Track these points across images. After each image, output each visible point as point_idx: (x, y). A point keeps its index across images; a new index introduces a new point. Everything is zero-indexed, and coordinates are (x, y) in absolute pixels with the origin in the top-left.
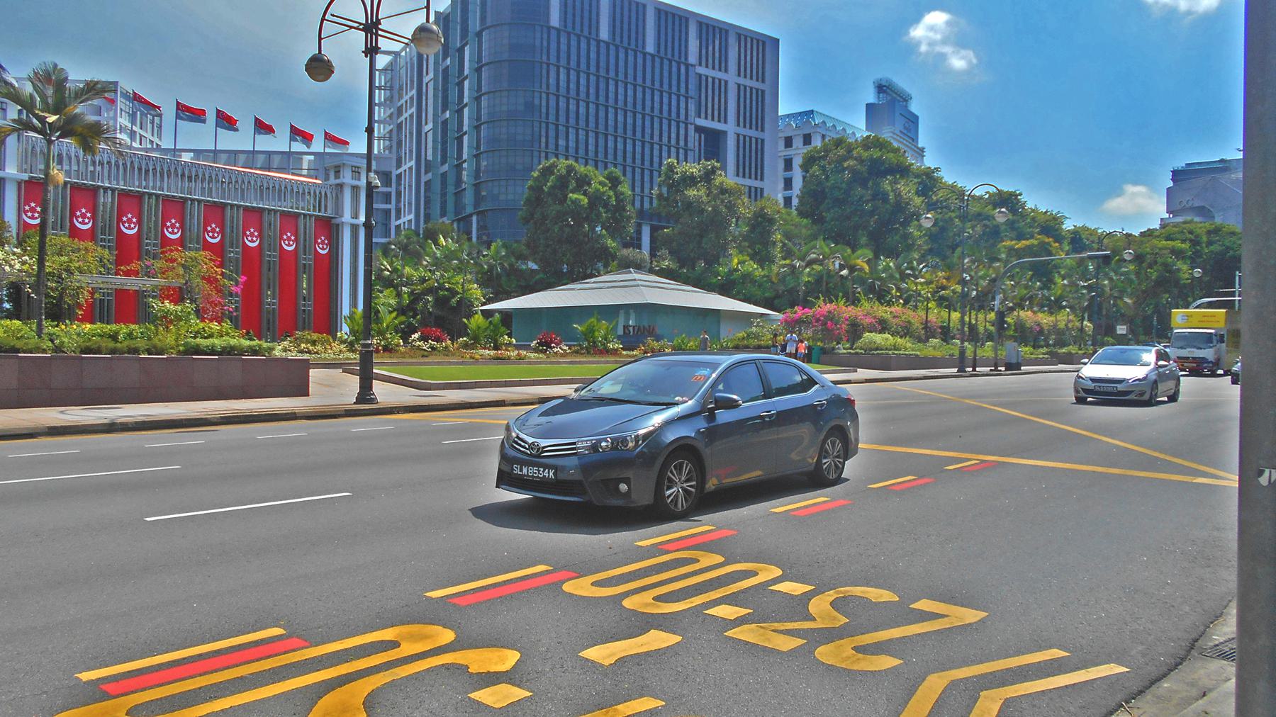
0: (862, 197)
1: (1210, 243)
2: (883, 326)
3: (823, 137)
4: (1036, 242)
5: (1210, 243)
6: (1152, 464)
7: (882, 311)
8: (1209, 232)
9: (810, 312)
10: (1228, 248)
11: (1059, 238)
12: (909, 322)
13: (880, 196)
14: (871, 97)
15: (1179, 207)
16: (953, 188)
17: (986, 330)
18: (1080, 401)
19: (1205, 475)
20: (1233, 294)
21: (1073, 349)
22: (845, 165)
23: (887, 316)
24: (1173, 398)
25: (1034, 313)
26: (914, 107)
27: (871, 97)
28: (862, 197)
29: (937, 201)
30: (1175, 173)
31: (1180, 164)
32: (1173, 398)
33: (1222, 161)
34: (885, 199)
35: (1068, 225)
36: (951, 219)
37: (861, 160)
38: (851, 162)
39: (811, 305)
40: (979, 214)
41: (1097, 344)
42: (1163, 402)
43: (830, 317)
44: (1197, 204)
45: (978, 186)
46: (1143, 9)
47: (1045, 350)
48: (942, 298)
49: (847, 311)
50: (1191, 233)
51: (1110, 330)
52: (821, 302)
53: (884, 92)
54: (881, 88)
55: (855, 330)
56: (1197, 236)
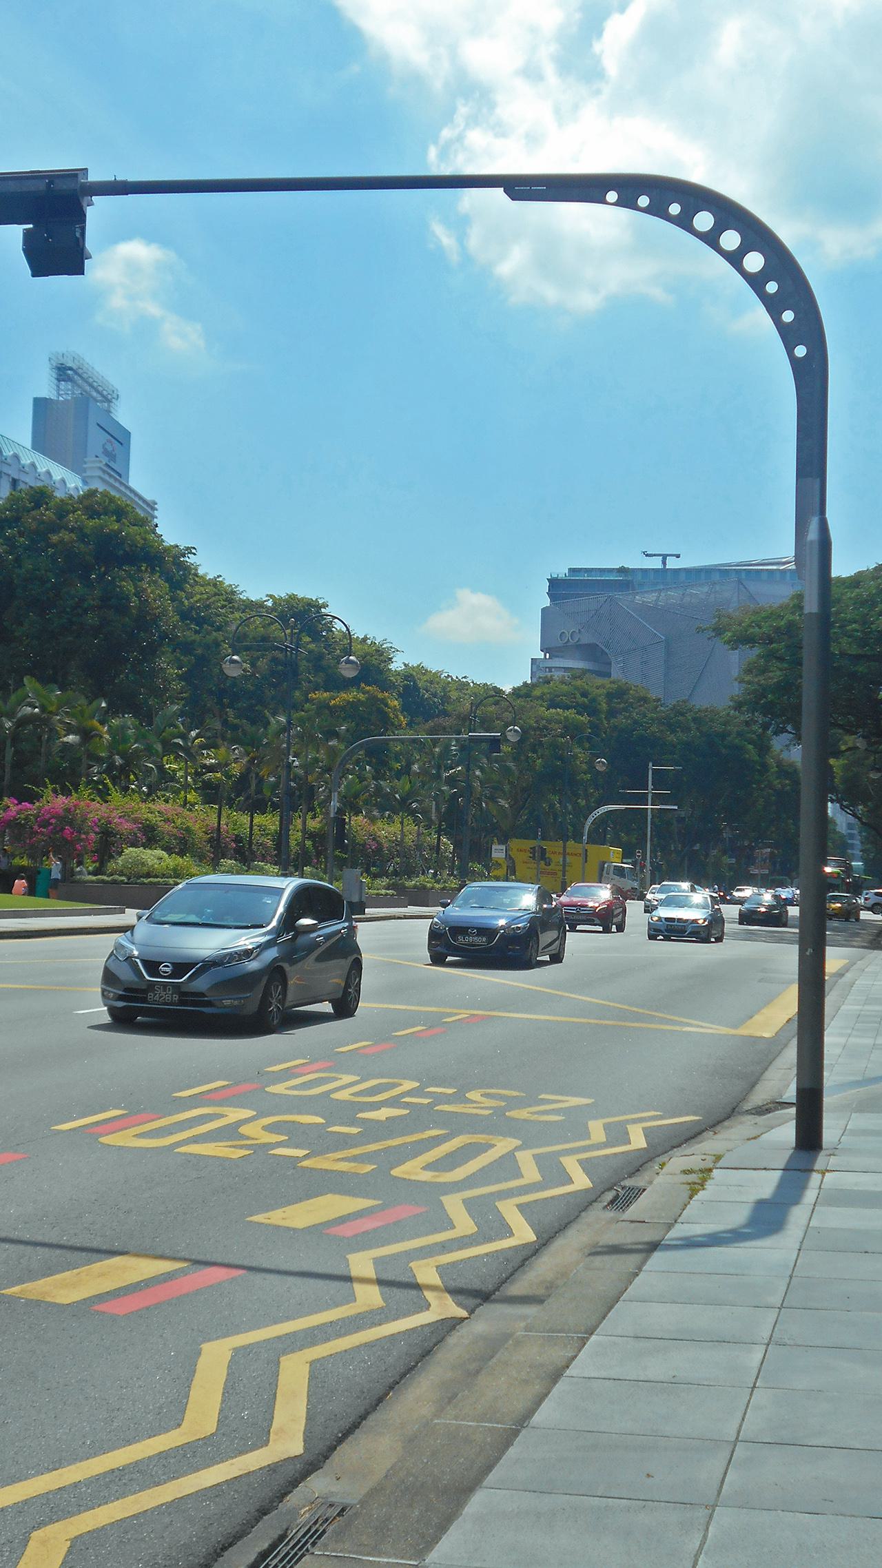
0: (82, 600)
1: (612, 713)
2: (149, 836)
3: (14, 482)
4: (361, 697)
5: (612, 713)
6: (638, 1017)
7: (156, 811)
8: (610, 696)
9: (32, 809)
10: (636, 722)
11: (386, 685)
12: (188, 830)
13: (113, 602)
14: (45, 387)
15: (560, 643)
16: (215, 583)
17: (301, 845)
18: (652, 937)
19: (691, 1025)
20: (642, 799)
21: (425, 880)
22: (55, 538)
23: (155, 819)
24: (557, 958)
25: (373, 820)
26: (123, 415)
27: (45, 387)
28: (82, 600)
29: (192, 608)
30: (554, 583)
31: (562, 571)
32: (557, 958)
33: (623, 570)
34: (123, 609)
35: (397, 665)
36: (217, 644)
37: (79, 530)
38: (66, 536)
39: (32, 797)
40: (265, 639)
41: (466, 876)
42: (544, 963)
43: (67, 818)
44: (586, 639)
45: (257, 584)
46: (344, 39)
47: (385, 881)
48: (207, 785)
49: (96, 811)
50: (584, 694)
51: (482, 854)
52: (48, 792)
53: (69, 379)
54: (63, 373)
55: (108, 844)
56: (594, 700)
